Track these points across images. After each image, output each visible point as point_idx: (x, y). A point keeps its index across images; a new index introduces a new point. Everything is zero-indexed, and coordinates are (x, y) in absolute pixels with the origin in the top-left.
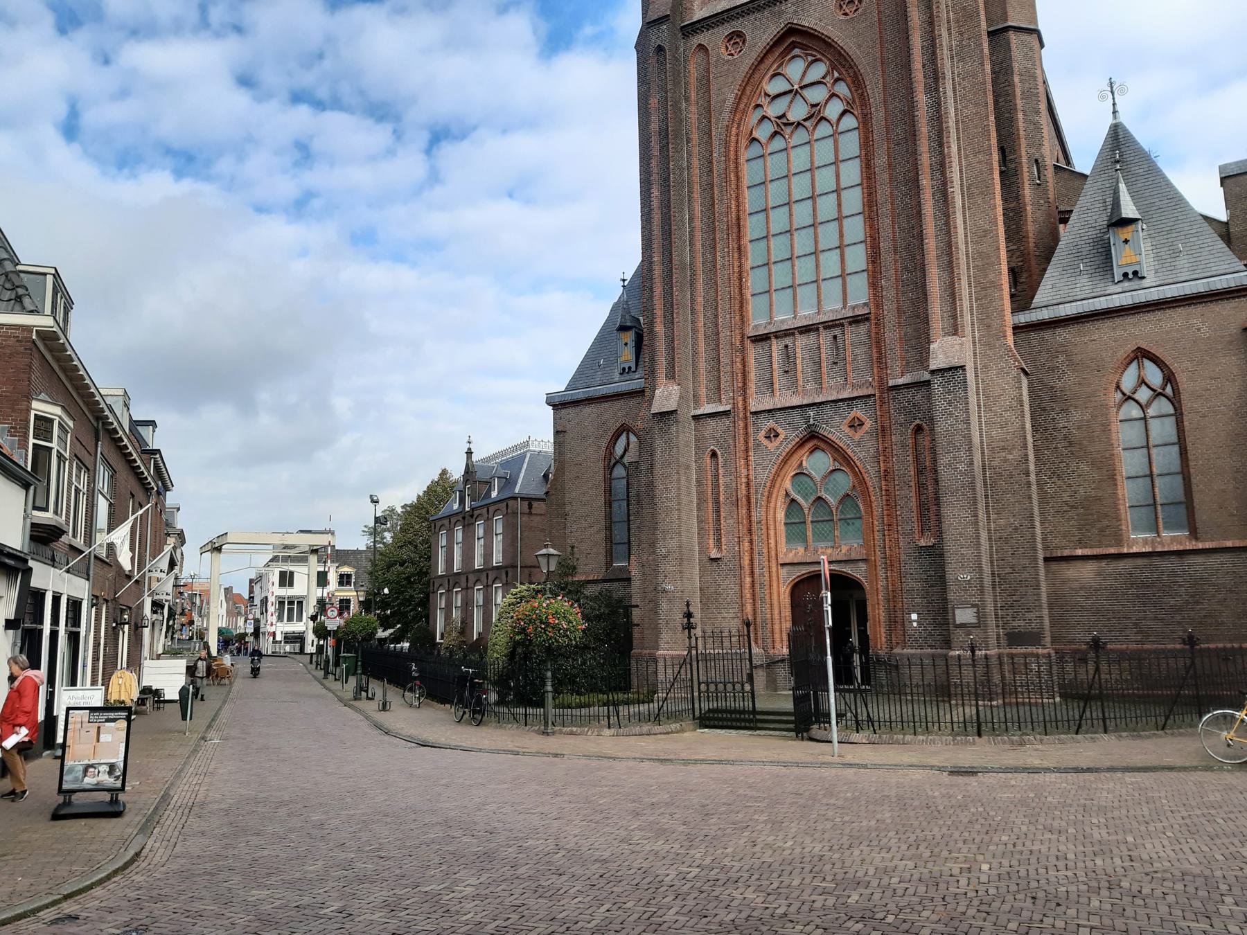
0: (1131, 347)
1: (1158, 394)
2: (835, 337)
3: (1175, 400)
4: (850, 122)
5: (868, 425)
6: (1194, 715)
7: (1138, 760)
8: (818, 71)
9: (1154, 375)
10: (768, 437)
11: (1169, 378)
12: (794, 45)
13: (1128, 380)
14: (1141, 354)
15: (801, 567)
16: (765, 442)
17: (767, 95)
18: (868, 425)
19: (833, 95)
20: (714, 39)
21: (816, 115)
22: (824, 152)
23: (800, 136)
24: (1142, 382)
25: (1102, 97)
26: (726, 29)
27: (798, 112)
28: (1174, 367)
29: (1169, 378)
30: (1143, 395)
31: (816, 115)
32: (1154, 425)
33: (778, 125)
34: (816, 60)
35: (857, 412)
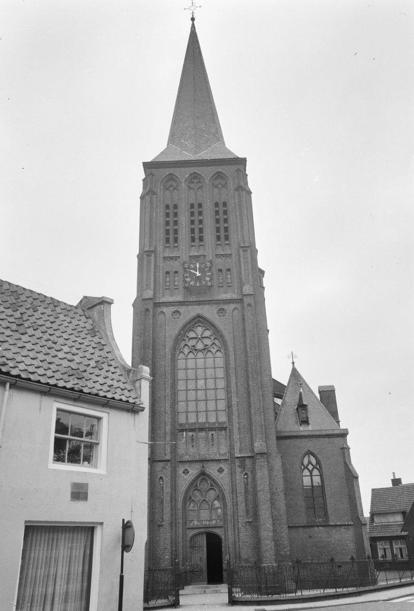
0: (306, 450)
1: (314, 467)
2: (212, 434)
3: (320, 470)
4: (219, 354)
5: (226, 470)
6: (246, 552)
7: (408, 593)
8: (207, 333)
9: (314, 461)
10: (184, 473)
11: (318, 462)
12: (199, 321)
13: (306, 461)
14: (310, 453)
15: (195, 530)
16: (183, 475)
17: (188, 337)
18: (226, 470)
19: (214, 343)
20: (168, 310)
21: (206, 349)
22: (210, 362)
23: (200, 355)
24: (310, 462)
25: (289, 358)
26: (173, 309)
27: (200, 346)
28: (321, 459)
29: (318, 462)
30: (310, 467)
31: (206, 349)
32: (217, 360)
33: (192, 349)
34: (208, 329)
35: (222, 465)
